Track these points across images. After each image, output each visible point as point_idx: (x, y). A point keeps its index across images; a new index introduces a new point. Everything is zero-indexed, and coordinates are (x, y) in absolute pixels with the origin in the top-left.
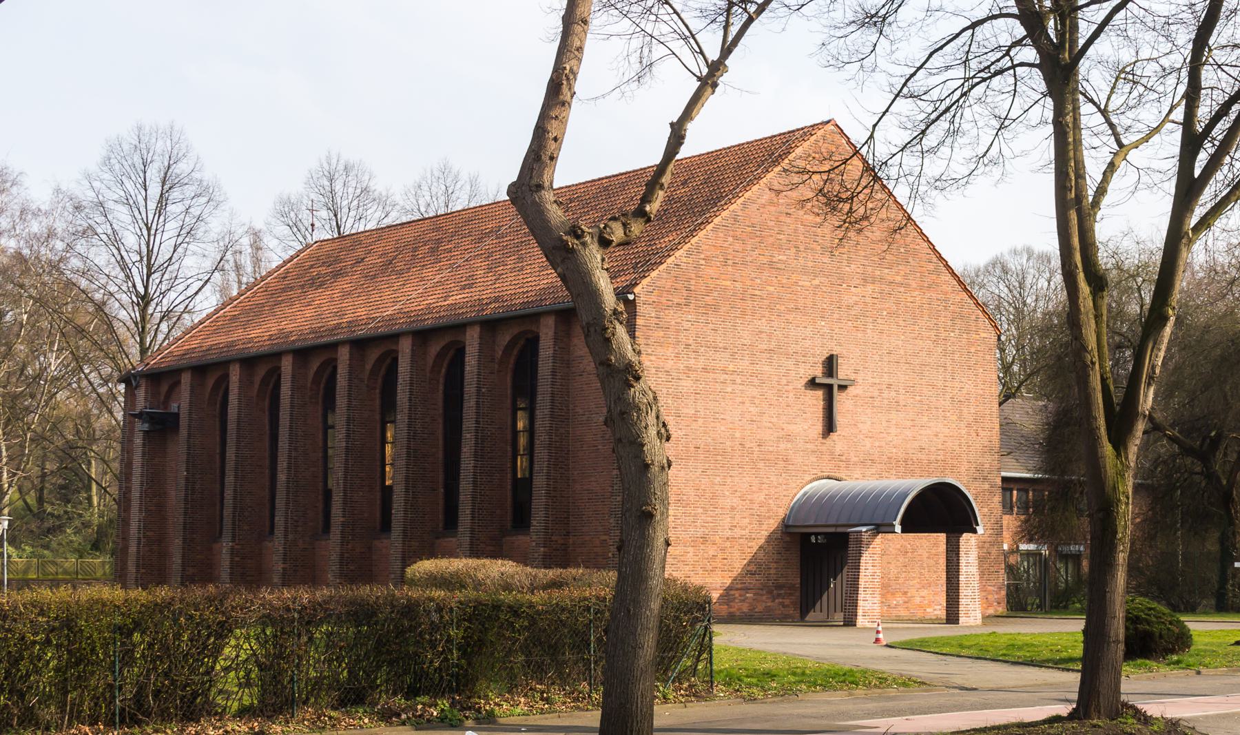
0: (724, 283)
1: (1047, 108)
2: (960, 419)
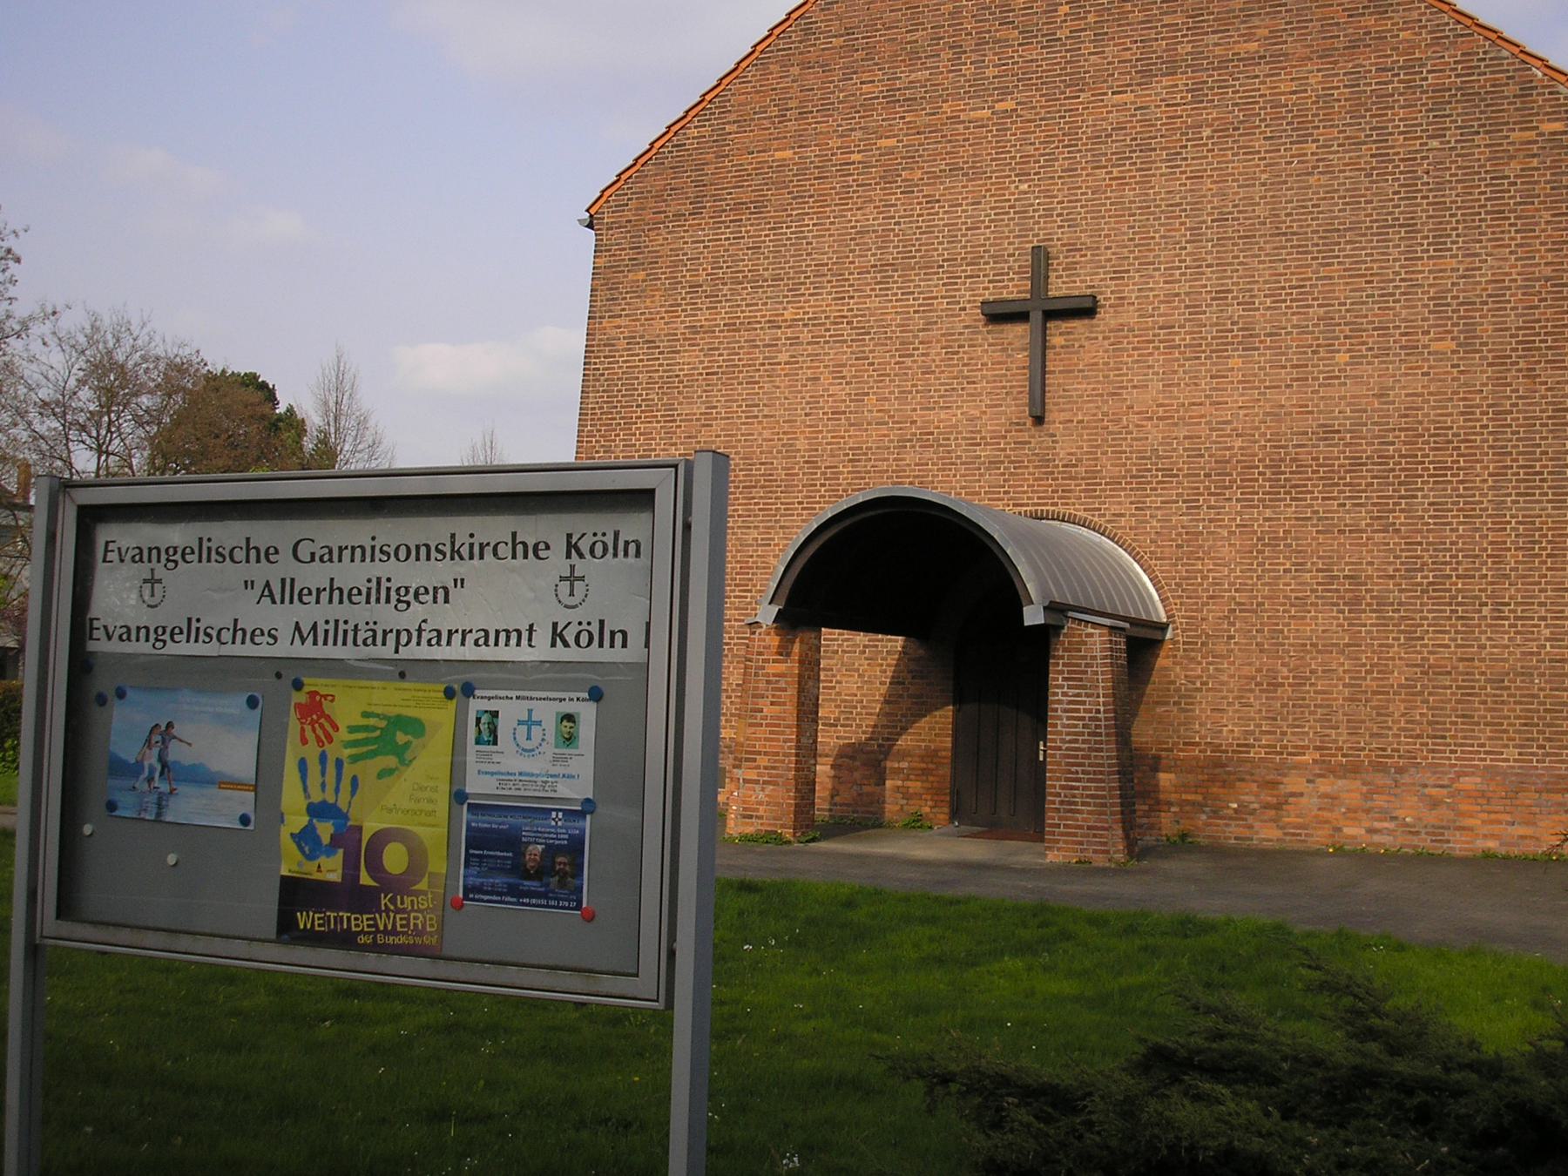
0: (778, 155)
1: (213, 790)
2: (1468, 344)
